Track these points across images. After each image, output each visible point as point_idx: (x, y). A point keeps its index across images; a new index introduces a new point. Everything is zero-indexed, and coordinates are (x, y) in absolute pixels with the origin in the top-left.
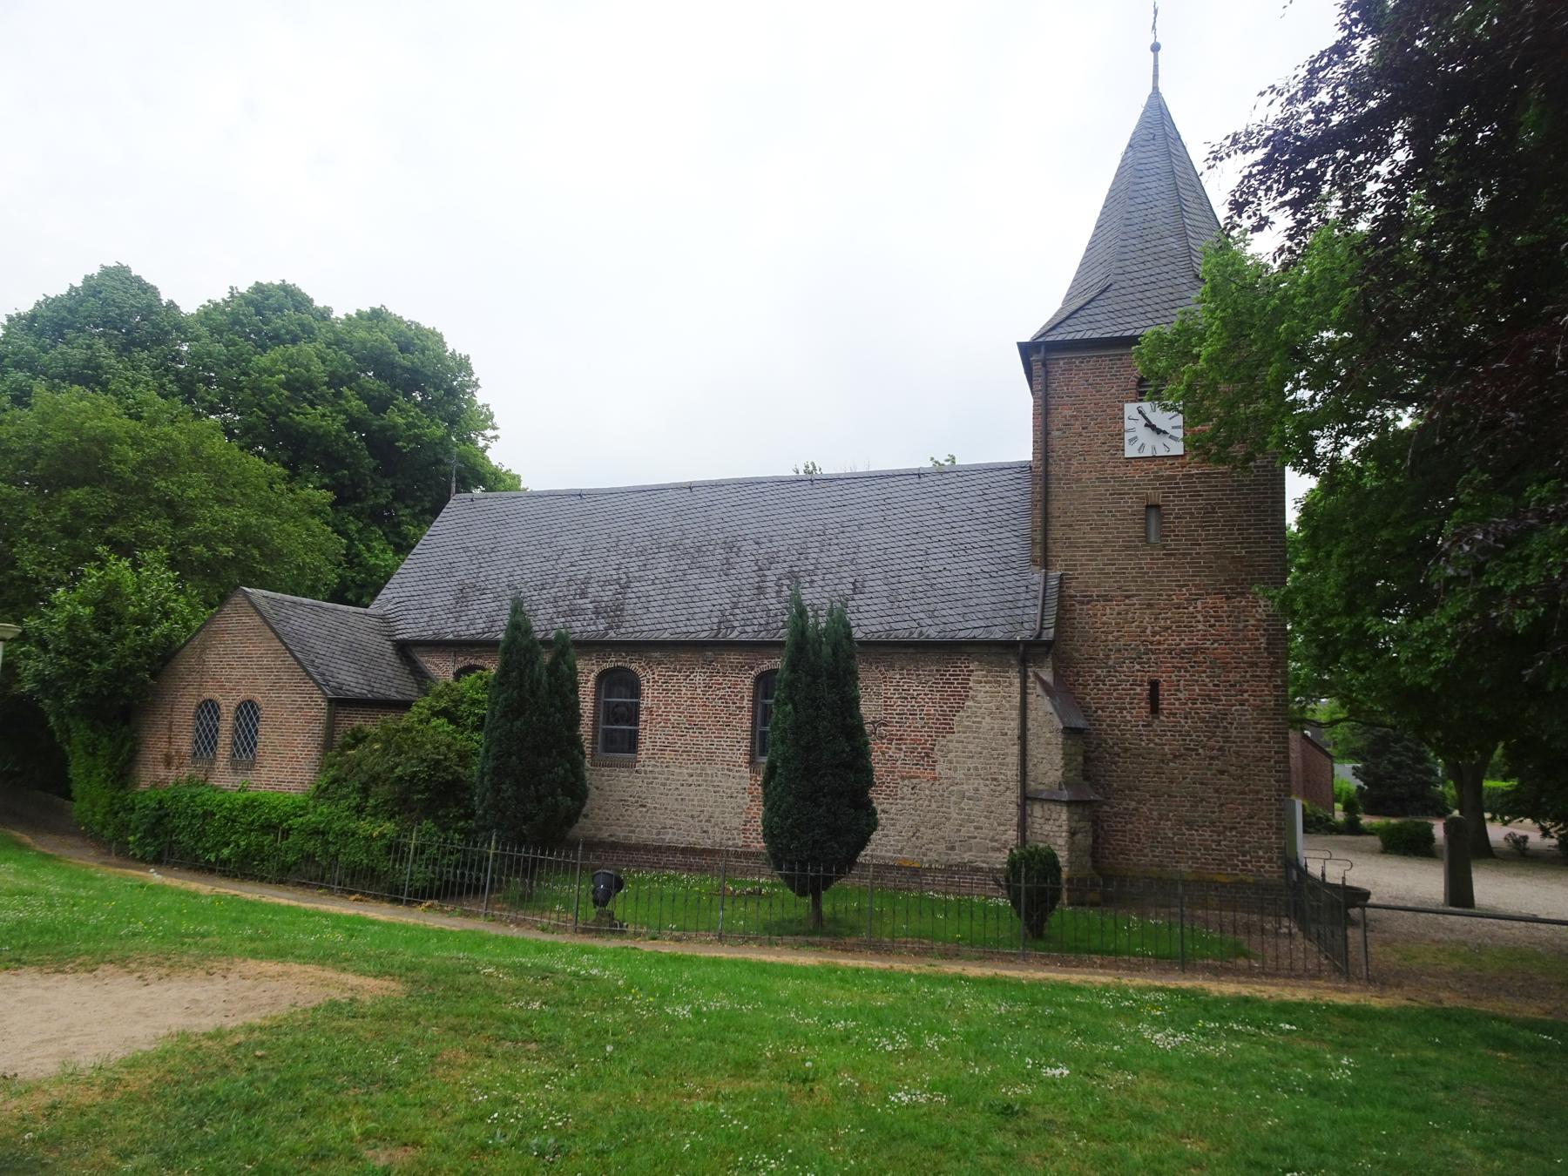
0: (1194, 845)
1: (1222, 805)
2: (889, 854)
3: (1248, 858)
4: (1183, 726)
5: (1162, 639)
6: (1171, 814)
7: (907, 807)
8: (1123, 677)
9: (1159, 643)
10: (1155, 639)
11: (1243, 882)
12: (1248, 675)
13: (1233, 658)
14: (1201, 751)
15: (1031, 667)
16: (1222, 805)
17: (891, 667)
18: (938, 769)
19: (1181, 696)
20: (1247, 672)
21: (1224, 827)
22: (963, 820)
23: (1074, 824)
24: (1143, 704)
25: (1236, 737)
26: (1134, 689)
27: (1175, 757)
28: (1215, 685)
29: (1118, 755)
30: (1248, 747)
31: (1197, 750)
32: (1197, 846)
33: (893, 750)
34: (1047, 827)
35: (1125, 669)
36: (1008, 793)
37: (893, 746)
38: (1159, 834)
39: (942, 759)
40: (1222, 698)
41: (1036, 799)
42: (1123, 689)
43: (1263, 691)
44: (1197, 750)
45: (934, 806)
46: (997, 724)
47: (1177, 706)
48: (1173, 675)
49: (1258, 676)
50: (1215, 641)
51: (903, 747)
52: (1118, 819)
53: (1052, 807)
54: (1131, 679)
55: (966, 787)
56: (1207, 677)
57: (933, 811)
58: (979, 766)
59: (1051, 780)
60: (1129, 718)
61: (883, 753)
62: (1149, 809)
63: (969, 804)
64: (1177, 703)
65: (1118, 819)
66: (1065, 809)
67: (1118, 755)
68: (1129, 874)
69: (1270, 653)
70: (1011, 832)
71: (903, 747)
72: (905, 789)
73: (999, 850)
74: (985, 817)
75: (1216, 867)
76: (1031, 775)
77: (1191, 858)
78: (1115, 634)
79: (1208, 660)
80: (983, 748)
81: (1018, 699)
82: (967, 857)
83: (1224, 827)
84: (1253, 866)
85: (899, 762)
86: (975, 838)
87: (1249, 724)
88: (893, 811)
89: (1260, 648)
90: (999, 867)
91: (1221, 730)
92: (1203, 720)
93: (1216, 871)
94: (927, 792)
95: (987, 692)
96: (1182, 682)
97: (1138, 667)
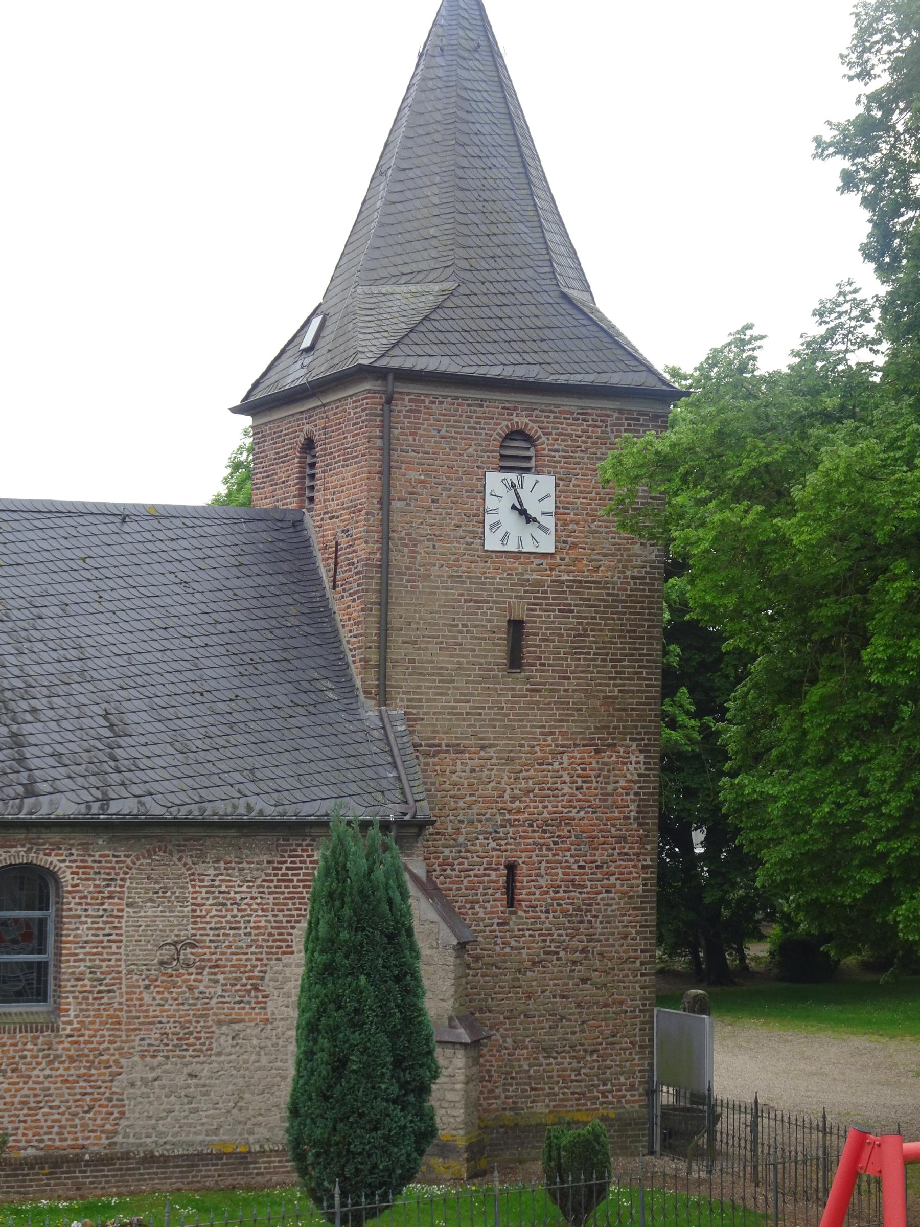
2: (200, 1138)
3: (609, 1087)
4: (544, 923)
5: (522, 805)
6: (528, 1040)
7: (227, 1066)
9: (519, 812)
10: (514, 806)
13: (601, 831)
14: (562, 954)
16: (583, 1023)
17: (202, 857)
20: (614, 849)
21: (585, 1051)
24: (498, 895)
25: (600, 934)
26: (489, 875)
27: (534, 963)
28: (580, 867)
30: (613, 946)
31: (557, 953)
32: (556, 1079)
33: (206, 982)
35: (478, 847)
38: (513, 1067)
39: (276, 993)
42: (476, 876)
43: (631, 873)
45: (264, 1060)
47: (537, 896)
48: (534, 854)
49: (626, 854)
50: (582, 808)
54: (485, 860)
60: (481, 915)
61: (191, 989)
62: (504, 1037)
64: (537, 892)
66: (461, 1053)
69: (639, 824)
72: (222, 1040)
75: (574, 1102)
77: (548, 1095)
78: (467, 799)
79: (573, 833)
83: (585, 1051)
85: (214, 1000)
91: (586, 925)
92: (565, 914)
93: (575, 1108)
94: (255, 1042)
96: (544, 864)
97: (493, 844)
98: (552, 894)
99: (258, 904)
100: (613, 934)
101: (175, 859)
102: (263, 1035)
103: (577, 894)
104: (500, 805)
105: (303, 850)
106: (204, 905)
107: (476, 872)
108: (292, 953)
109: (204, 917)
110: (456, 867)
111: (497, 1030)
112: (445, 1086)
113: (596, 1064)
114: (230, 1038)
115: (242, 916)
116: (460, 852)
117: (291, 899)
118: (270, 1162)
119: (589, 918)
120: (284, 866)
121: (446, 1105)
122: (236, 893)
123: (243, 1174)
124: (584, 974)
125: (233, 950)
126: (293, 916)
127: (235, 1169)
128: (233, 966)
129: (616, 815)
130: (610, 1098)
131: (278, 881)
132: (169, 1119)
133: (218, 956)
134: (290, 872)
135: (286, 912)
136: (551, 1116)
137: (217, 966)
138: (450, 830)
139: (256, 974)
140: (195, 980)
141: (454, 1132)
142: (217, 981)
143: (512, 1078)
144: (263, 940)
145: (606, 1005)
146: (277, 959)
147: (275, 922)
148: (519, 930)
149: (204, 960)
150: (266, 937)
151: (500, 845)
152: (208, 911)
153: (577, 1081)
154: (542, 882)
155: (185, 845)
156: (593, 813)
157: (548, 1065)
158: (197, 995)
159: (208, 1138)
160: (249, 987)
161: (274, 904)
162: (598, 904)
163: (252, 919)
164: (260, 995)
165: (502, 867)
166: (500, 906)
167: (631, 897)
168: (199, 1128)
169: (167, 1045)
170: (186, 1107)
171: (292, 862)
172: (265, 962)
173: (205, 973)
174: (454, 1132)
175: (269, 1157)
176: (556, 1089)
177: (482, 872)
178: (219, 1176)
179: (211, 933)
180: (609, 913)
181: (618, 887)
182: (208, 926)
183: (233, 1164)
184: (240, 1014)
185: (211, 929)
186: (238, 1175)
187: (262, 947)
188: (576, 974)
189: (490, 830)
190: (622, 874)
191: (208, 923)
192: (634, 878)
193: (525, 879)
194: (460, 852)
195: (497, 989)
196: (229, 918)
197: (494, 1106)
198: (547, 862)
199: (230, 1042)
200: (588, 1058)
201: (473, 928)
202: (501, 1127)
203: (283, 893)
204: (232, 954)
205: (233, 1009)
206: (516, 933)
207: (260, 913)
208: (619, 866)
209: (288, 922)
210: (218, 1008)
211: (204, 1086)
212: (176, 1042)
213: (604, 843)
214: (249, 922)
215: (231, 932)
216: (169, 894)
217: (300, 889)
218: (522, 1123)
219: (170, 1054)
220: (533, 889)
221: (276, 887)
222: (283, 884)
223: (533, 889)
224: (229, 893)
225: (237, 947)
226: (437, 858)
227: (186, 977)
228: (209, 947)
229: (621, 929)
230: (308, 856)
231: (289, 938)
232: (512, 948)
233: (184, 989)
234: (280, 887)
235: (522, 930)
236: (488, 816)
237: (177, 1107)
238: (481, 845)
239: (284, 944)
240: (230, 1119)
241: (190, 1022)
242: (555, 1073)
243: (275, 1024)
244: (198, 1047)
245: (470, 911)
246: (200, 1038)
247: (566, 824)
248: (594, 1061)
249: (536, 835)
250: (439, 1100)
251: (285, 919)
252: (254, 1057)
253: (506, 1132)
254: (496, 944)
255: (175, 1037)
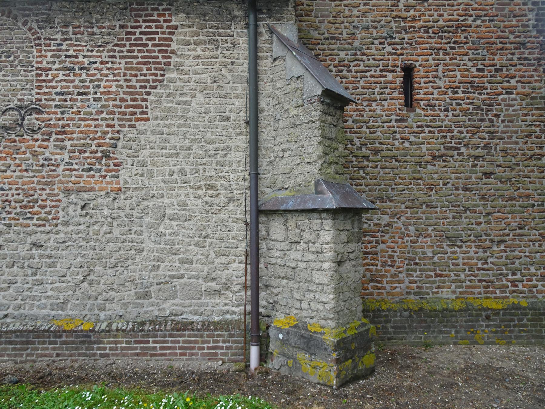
0: (458, 265)
1: (488, 214)
2: (44, 312)
3: (519, 276)
4: (444, 121)
5: (417, 14)
6: (430, 228)
7: (75, 236)
8: (372, 61)
9: (414, 20)
10: (409, 14)
11: (516, 307)
12: (515, 57)
13: (499, 37)
14: (463, 150)
15: (262, 20)
16: (488, 214)
17: (48, 21)
18: (123, 174)
19: (440, 83)
20: (513, 54)
21: (492, 241)
22: (162, 251)
23: (341, 248)
24: (395, 95)
25: (503, 132)
26: (385, 77)
27: (434, 157)
28: (478, 70)
29: (367, 158)
30: (517, 143)
31: (458, 149)
32: (461, 266)
33: (51, 149)
34: (296, 255)
35: (374, 51)
36: (231, 206)
37: (52, 143)
38: (416, 254)
39: (129, 161)
40: (488, 85)
41: (275, 212)
42: (372, 76)
43: (532, 76)
44: (458, 149)
45: (117, 232)
46: (214, 105)
47: (436, 96)
48: (430, 58)
49: (526, 59)
50: (478, 17)
51: (68, 143)
52: (368, 238)
53: (303, 221)
54: (381, 63)
55: (166, 201)
56: (469, 60)
57: (116, 240)
58: (187, 169)
59: (300, 180)
60: (379, 112)
61: (35, 155)
62: (406, 225)
63: (172, 227)
64: (436, 92)
65: (368, 238)
66: (328, 223)
67: (367, 158)
68: (384, 307)
69: (539, 31)
70: (235, 265)
71: (68, 143)
72: (70, 210)
73: (217, 293)
74: (197, 244)
75: (482, 290)
76: (266, 178)
77: (454, 281)
78: (362, 7)
79: (470, 40)
80: (193, 141)
81: (246, 66)
82: (168, 307)
83: (492, 241)
84: (524, 286)
85: (62, 167)
86: (182, 277)
87: (518, 115)
88: (51, 243)
89: (527, 26)
90: (217, 319)
91: (487, 123)
92: (465, 112)
93: (483, 295)
94: (106, 212)
95: (198, 57)
96: (441, 67)
97: (389, 49)
98: (451, 95)
99: (109, 69)
100: (517, 132)
101: (20, 24)
102: (116, 205)
103: (476, 95)
104: (395, 13)
105: (159, 15)
106: (50, 69)
107: (372, 73)
108: (148, 119)
109: (51, 81)
110: (353, 69)
111: (399, 218)
112: (312, 265)
113: (504, 255)
114: (79, 207)
115: (91, 81)
116: (356, 54)
117: (145, 63)
118: (116, 343)
119: (490, 116)
120: (138, 31)
121: (314, 288)
122: (84, 57)
123: (85, 355)
124: (486, 169)
125: (82, 116)
126: (148, 81)
127: (77, 349)
128: (81, 132)
129: (514, 23)
130: (520, 287)
131: (131, 45)
132: (11, 291)
133: (65, 122)
134: (144, 37)
135: (140, 78)
136: (459, 302)
137: (64, 133)
138: (345, 35)
139: (107, 141)
140: (40, 147)
141: (323, 323)
142: (63, 148)
143: (416, 264)
144: (115, 106)
145: (512, 199)
146: (131, 126)
147: (128, 87)
148: (418, 127)
149: (49, 126)
150: (118, 103)
151: (397, 49)
152: (54, 77)
153: (483, 269)
154: (440, 83)
155: (30, 10)
156: (490, 21)
157: (453, 253)
158: (41, 161)
159: (53, 313)
160: (99, 154)
161: (126, 69)
162: (499, 104)
163: (102, 84)
164: (111, 162)
165: (399, 69)
166: (398, 104)
167: (533, 98)
168: (43, 301)
169: (10, 213)
170: (30, 278)
171: (147, 27)
172: (117, 128)
173: (52, 139)
174: (323, 323)
175: (115, 336)
176: (463, 277)
177: (378, 73)
178: (58, 355)
179: (57, 97)
180: (510, 112)
181: (520, 89)
182: (54, 91)
183: (73, 342)
184: (89, 183)
185: (57, 94)
186: (79, 355)
187: (113, 113)
188: (478, 168)
189: (385, 35)
190: (523, 77)
191: (53, 87)
192: (536, 81)
193: (423, 80)
194: (356, 54)
195: (397, 180)
196: (77, 82)
197: (398, 290)
198: (445, 65)
199: (79, 211)
200: (495, 248)
201: (371, 123)
202: (405, 310)
203: (136, 57)
204: (80, 119)
205: (81, 176)
206: (415, 129)
207: (111, 77)
208: (520, 70)
209: (141, 87)
210: (65, 176)
211: (50, 257)
212: (19, 210)
213: (502, 49)
214: (99, 86)
215: (79, 97)
216: (12, 58)
217: (156, 54)
218: (427, 307)
219: (13, 222)
220: (431, 89)
221: (128, 51)
222: (136, 49)
223: (431, 89)
224: (77, 57)
225: (86, 113)
226: (333, 60)
227: (31, 143)
228: (55, 113)
229: (524, 128)
230: (165, 21)
231: (143, 104)
232: (411, 143)
233: (28, 155)
234: (133, 51)
235: (421, 126)
236: (382, 23)
237: (20, 279)
238: (377, 49)
239: (138, 111)
240: (78, 292)
241: (35, 189)
242: (460, 261)
243: (128, 194)
244: (43, 215)
245: (367, 109)
246: (46, 207)
247: (463, 31)
248: (501, 251)
249: (432, 40)
250: (306, 281)
251: (138, 85)
252: (105, 228)
253: (411, 316)
254: (395, 139)
255: (18, 205)
